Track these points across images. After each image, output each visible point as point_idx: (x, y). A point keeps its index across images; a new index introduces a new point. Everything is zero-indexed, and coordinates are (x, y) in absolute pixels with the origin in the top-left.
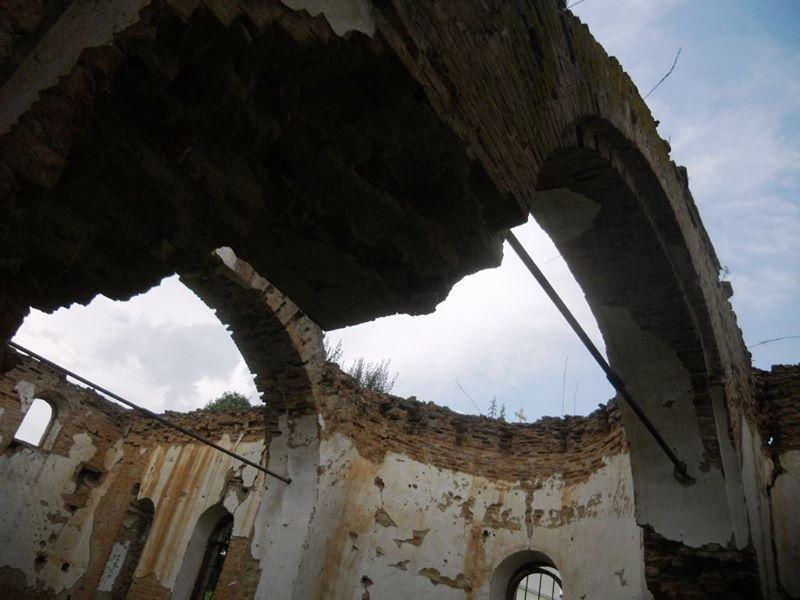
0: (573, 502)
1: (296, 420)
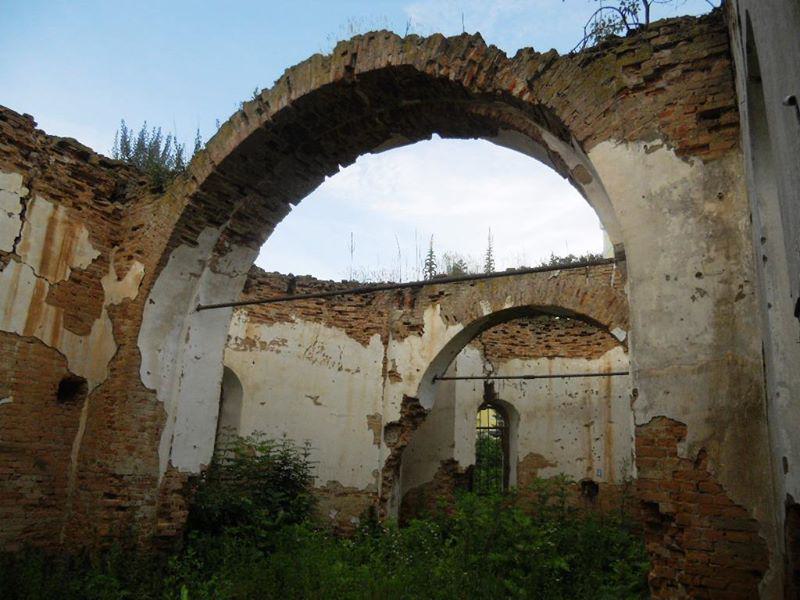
0: (256, 336)
1: (234, 247)
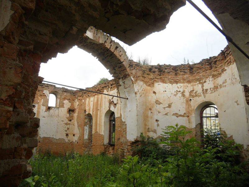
1: (125, 80)
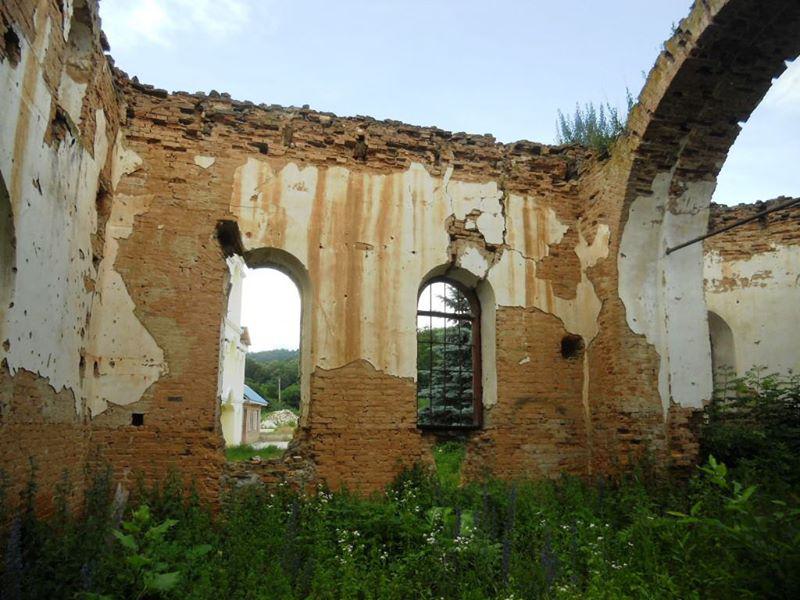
1: (689, 184)
